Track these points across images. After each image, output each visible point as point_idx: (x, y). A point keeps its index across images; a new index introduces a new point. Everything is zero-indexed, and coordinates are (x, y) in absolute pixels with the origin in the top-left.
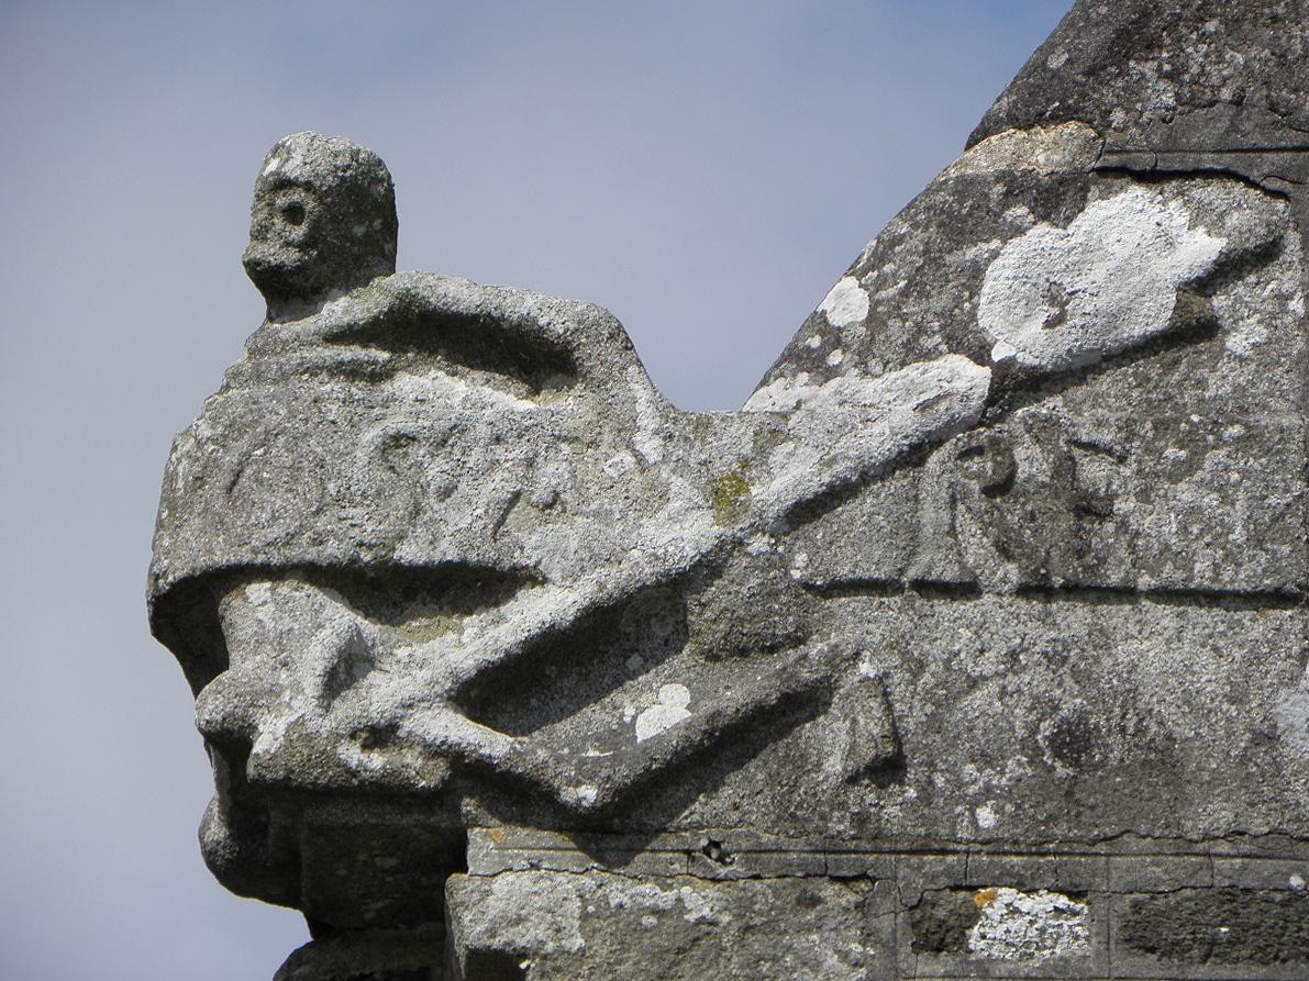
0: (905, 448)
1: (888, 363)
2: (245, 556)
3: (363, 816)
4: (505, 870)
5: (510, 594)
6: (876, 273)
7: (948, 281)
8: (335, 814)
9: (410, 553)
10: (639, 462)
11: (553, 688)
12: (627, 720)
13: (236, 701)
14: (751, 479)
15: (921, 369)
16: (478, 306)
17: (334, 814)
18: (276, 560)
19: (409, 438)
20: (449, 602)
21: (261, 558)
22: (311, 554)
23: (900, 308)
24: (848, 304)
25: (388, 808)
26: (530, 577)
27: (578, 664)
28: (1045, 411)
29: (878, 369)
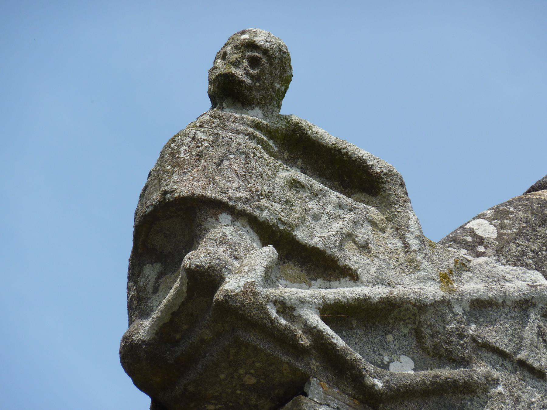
0: (523, 300)
1: (508, 261)
2: (224, 198)
3: (264, 346)
4: (326, 405)
5: (338, 278)
6: (499, 222)
7: (538, 239)
8: (253, 339)
9: (301, 235)
10: (406, 247)
11: (353, 331)
12: (386, 363)
13: (217, 261)
14: (453, 280)
15: (523, 271)
16: (333, 144)
17: (253, 338)
18: (240, 206)
19: (301, 185)
20: (306, 270)
21: (231, 203)
22: (257, 213)
23: (516, 240)
24: (486, 229)
25: (278, 348)
26: (353, 276)
27: (365, 326)
28: (462, 342)
29: (504, 262)
